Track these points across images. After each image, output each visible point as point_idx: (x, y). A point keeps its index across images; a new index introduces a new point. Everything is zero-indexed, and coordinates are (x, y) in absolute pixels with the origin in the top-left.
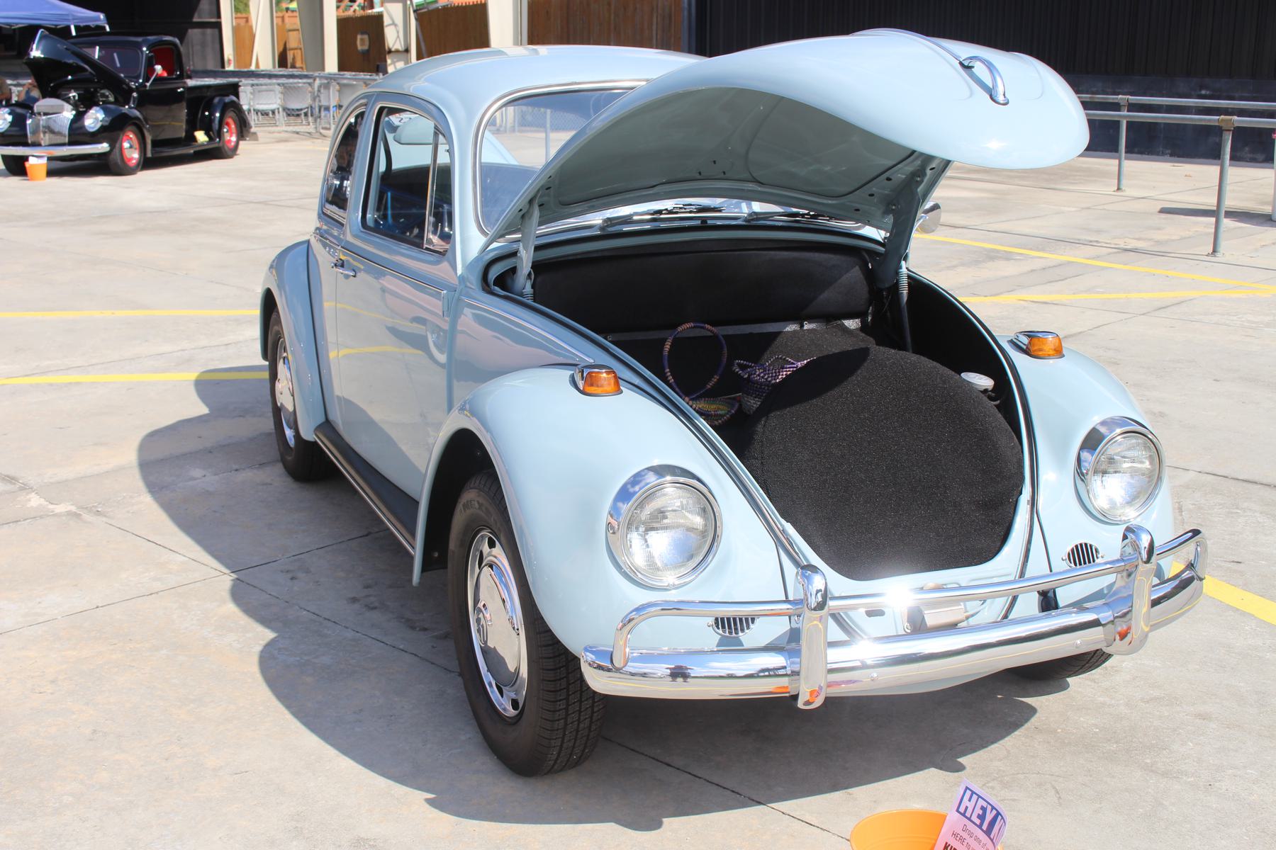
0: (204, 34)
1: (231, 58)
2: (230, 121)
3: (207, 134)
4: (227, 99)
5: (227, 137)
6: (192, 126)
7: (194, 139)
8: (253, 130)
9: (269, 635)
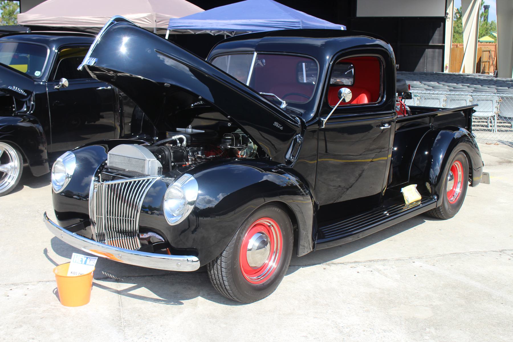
0: (434, 52)
1: (448, 65)
2: (458, 165)
3: (421, 189)
4: (457, 134)
5: (450, 185)
6: (399, 179)
7: (401, 199)
8: (484, 170)
9: (416, 185)
